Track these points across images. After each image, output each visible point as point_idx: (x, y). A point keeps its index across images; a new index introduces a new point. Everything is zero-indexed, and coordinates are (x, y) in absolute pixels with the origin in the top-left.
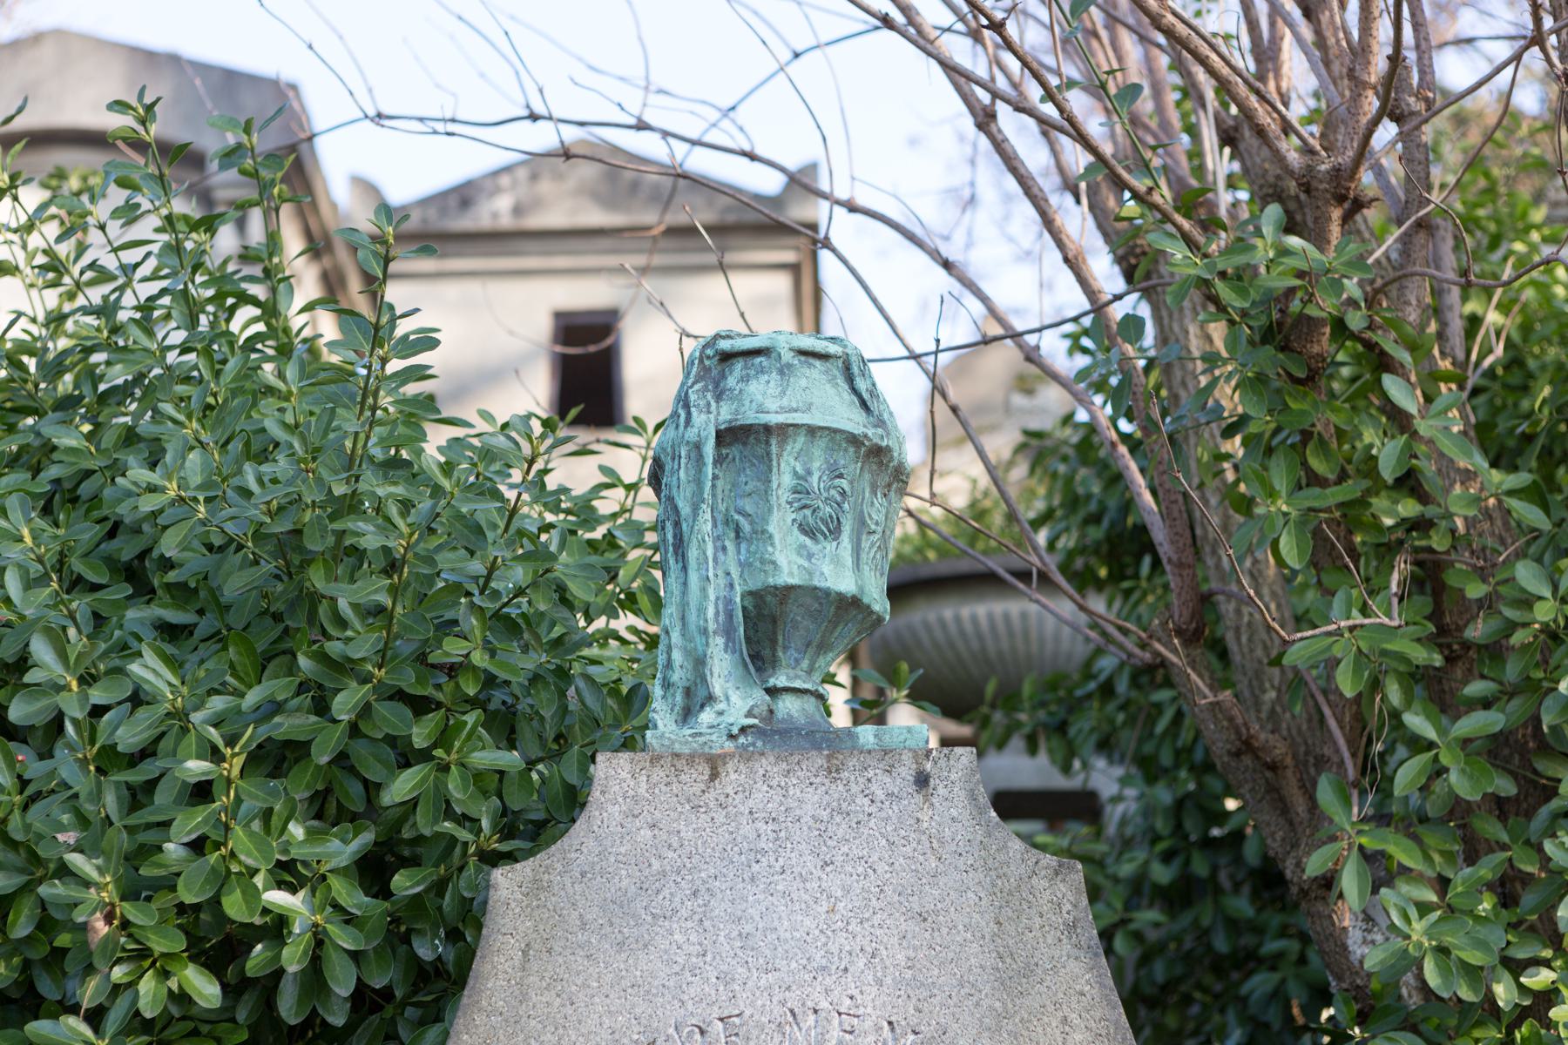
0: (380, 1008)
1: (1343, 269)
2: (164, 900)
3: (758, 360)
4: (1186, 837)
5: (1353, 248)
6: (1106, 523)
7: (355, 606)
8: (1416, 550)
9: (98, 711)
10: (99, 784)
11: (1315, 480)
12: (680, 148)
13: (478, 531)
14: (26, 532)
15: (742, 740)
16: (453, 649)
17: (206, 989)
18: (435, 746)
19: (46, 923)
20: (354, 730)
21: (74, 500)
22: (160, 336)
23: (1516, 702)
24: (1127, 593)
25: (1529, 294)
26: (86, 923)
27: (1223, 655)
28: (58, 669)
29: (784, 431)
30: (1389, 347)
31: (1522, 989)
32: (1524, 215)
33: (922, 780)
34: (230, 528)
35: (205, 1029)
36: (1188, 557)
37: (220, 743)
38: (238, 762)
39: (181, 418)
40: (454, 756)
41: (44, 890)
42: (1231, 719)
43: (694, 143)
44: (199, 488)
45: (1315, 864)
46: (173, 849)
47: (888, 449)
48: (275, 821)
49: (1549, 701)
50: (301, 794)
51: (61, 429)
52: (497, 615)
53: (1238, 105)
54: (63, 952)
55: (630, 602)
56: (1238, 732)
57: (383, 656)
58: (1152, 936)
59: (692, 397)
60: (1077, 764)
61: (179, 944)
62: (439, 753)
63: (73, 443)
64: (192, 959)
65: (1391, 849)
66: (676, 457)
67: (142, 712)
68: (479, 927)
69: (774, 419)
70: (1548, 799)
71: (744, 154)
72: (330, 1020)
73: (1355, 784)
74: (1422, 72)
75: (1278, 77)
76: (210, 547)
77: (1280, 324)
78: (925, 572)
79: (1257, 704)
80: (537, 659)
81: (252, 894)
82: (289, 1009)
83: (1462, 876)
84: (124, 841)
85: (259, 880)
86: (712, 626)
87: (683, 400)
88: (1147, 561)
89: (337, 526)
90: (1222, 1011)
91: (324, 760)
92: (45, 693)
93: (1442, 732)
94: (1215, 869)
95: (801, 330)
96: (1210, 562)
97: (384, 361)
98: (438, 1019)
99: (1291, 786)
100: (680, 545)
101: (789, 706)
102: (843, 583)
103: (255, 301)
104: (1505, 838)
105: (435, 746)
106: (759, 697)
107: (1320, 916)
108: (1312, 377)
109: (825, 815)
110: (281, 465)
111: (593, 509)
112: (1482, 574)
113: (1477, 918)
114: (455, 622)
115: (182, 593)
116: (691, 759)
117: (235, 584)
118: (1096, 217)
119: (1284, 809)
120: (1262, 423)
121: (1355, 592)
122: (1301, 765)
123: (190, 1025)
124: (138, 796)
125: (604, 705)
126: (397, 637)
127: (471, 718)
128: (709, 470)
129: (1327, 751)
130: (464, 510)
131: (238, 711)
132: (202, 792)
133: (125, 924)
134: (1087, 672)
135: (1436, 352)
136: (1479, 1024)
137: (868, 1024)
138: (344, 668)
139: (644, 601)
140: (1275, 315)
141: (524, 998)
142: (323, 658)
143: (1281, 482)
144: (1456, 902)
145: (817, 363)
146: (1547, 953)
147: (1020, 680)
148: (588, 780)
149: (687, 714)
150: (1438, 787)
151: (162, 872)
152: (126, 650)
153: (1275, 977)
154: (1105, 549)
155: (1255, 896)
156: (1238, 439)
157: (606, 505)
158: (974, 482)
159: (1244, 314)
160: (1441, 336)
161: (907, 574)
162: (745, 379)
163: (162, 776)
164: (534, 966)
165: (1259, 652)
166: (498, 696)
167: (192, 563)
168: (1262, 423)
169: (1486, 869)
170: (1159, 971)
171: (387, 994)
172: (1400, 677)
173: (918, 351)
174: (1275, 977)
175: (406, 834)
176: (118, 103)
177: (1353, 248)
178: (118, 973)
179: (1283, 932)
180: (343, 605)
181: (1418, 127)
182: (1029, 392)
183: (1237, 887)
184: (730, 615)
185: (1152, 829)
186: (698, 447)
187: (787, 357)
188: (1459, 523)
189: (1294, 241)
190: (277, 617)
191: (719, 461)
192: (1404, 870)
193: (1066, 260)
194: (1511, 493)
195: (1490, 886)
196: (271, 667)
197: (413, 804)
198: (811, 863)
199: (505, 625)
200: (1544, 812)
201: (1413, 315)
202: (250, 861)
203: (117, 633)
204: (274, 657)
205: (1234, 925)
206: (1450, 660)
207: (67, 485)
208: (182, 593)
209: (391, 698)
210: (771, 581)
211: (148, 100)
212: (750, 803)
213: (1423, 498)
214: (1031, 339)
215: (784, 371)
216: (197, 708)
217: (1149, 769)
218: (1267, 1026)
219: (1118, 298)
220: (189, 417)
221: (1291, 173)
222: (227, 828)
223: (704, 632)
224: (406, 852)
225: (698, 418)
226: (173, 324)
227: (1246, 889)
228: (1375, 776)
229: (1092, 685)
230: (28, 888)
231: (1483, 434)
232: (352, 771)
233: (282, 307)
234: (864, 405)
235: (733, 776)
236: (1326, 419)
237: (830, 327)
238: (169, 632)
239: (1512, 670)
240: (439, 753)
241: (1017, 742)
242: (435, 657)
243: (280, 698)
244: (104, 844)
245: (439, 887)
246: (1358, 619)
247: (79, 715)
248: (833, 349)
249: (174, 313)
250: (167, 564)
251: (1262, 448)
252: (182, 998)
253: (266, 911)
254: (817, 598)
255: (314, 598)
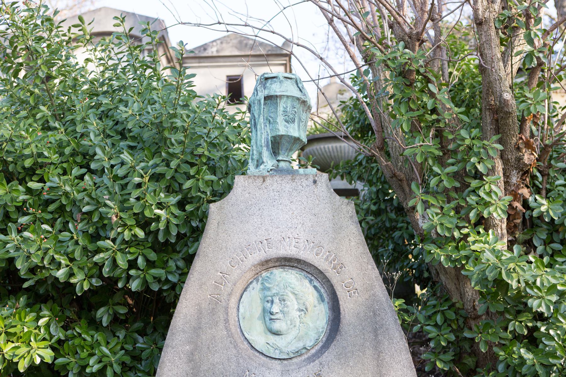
0: (183, 238)
1: (419, 58)
2: (130, 212)
3: (274, 79)
4: (379, 199)
5: (421, 52)
6: (360, 123)
7: (176, 140)
8: (436, 127)
9: (112, 166)
10: (113, 184)
11: (411, 110)
12: (256, 31)
13: (206, 122)
14: (94, 123)
15: (271, 172)
16: (200, 151)
17: (141, 234)
18: (196, 174)
19: (101, 218)
20: (176, 171)
21: (107, 117)
22: (127, 75)
23: (460, 164)
24: (365, 140)
25: (464, 67)
26: (111, 218)
27: (389, 155)
28: (103, 156)
29: (281, 97)
30: (430, 76)
31: (461, 233)
32: (463, 47)
33: (315, 182)
34: (145, 121)
35: (141, 243)
36: (380, 130)
37: (143, 174)
38: (147, 178)
39: (133, 95)
40: (200, 177)
41: (100, 210)
42: (390, 169)
43: (260, 30)
44: (137, 112)
45: (411, 204)
46: (132, 200)
47: (306, 101)
48: (157, 193)
49: (468, 164)
50: (163, 186)
51: (104, 98)
52: (211, 143)
53: (394, 17)
54: (106, 224)
55: (244, 141)
56: (392, 172)
57: (183, 152)
58: (371, 223)
59: (258, 89)
60: (353, 182)
61: (134, 222)
62: (197, 176)
63: (107, 102)
64: (137, 226)
65: (429, 200)
66: (254, 103)
67: (124, 167)
68: (207, 218)
69: (278, 94)
70: (468, 188)
71: (272, 32)
72: (171, 241)
73: (421, 184)
74: (439, 8)
75: (403, 11)
76: (140, 127)
77: (403, 71)
78: (316, 137)
79: (397, 166)
80: (219, 154)
81: (151, 211)
82: (161, 238)
83: (446, 206)
84: (120, 198)
85: (153, 207)
86: (263, 145)
87: (256, 90)
88: (370, 132)
89: (171, 121)
90: (388, 241)
91: (169, 178)
92: (100, 162)
93: (442, 171)
94: (386, 207)
95: (286, 72)
96: (385, 131)
97: (182, 80)
98: (198, 241)
99: (405, 183)
100: (255, 125)
101: (282, 164)
102: (296, 134)
103: (151, 68)
104: (457, 197)
105: (196, 174)
106: (275, 162)
107: (412, 216)
108: (410, 85)
109: (291, 190)
110: (157, 106)
111: (235, 119)
112: (452, 133)
113: (450, 216)
114: (200, 145)
115: (134, 138)
116: (258, 177)
117: (146, 135)
118: (358, 47)
119: (403, 191)
120: (399, 96)
121: (421, 137)
122: (407, 180)
123: (137, 242)
124: (123, 187)
125: (237, 164)
126: (186, 148)
127: (205, 168)
128: (262, 106)
129: (414, 176)
130: (203, 117)
131: (148, 166)
132: (139, 186)
133: (121, 218)
134: (356, 160)
135: (441, 79)
136: (450, 242)
137: (302, 241)
138: (173, 155)
139: (247, 140)
140: (402, 69)
141: (218, 235)
142: (168, 153)
143: (403, 110)
144: (445, 213)
145: (289, 80)
146: (467, 225)
147: (339, 162)
148: (233, 183)
149: (257, 166)
150: (441, 185)
151: (130, 205)
152: (120, 152)
153: (401, 232)
154: (360, 130)
155: (396, 213)
156: (392, 100)
157: (238, 118)
158: (329, 115)
159: (394, 69)
160: (443, 75)
161: (311, 137)
162: (271, 84)
163: (128, 182)
164: (220, 227)
165: (397, 153)
166: (212, 163)
167: (136, 130)
168: (399, 96)
169: (452, 205)
170: (373, 231)
171: (185, 235)
172: (432, 158)
173: (314, 79)
174: (401, 232)
175: (189, 196)
176: (115, 17)
177: (421, 52)
178: (119, 230)
179: (403, 222)
180: (173, 140)
181: (438, 22)
182: (342, 94)
183: (392, 211)
184: (268, 142)
185: (371, 197)
186: (260, 101)
187: (282, 78)
188: (447, 120)
189: (407, 50)
190: (157, 144)
191: (265, 104)
192: (433, 205)
193: (351, 56)
194: (460, 113)
195: (453, 209)
196: (155, 156)
197: (190, 189)
198: (288, 202)
199: (213, 145)
200: (467, 191)
201: (436, 69)
202: (151, 202)
203: (118, 148)
204: (157, 153)
205: (391, 220)
206: (444, 154)
207: (105, 113)
208: (134, 138)
209: (185, 163)
210: (278, 134)
211: (123, 17)
212: (273, 187)
213: (438, 114)
214: (342, 76)
215: (281, 82)
216: (137, 166)
217: (370, 183)
218: (399, 244)
219: (363, 66)
220: (135, 95)
221: (406, 33)
222: (145, 194)
223: (261, 146)
224: (189, 201)
225: (260, 94)
226: (131, 73)
227: (394, 212)
228: (425, 183)
229: (357, 163)
230: (97, 209)
231: (453, 99)
232: (176, 181)
233: (158, 69)
234: (300, 90)
235: (268, 181)
236: (415, 94)
237: (293, 72)
238: (131, 148)
239: (459, 156)
240: (197, 176)
241: (338, 177)
242: (195, 153)
243: (158, 163)
244: (115, 198)
245: (198, 209)
246: (421, 143)
247: (108, 167)
248: (293, 77)
249: (131, 70)
250: (130, 131)
251: (398, 102)
252: (135, 236)
253: (155, 215)
254: (289, 138)
255: (166, 139)
